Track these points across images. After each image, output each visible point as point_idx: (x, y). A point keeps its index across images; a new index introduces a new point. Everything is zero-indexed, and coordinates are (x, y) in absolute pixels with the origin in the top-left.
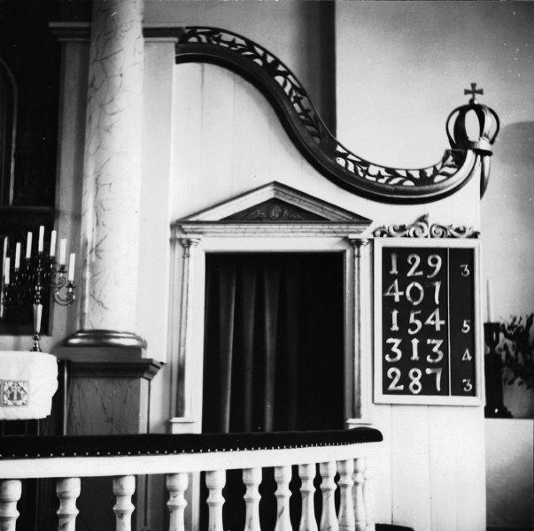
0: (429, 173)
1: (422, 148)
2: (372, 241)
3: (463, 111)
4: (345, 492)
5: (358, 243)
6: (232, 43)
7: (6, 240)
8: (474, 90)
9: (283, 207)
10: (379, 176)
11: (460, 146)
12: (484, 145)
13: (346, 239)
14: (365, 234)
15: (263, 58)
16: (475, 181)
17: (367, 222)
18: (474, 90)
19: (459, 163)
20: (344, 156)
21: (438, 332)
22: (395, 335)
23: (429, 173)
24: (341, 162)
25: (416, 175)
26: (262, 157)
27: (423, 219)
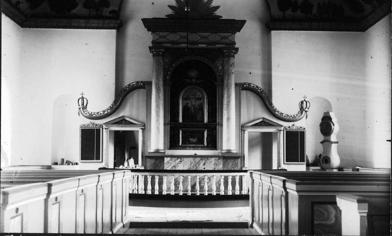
0: (93, 113)
1: (293, 110)
2: (284, 130)
3: (302, 102)
4: (355, 199)
5: (281, 131)
6: (254, 87)
7: (181, 120)
8: (305, 97)
9: (264, 123)
10: (285, 116)
11: (302, 109)
12: (307, 110)
13: (278, 129)
14: (282, 128)
15: (260, 90)
16: (305, 117)
17: (282, 126)
18: (305, 97)
19: (302, 113)
20: (278, 112)
21: (206, 124)
22: (206, 126)
23: (93, 113)
24: (277, 113)
25: (292, 116)
26: (257, 112)
27: (293, 125)
